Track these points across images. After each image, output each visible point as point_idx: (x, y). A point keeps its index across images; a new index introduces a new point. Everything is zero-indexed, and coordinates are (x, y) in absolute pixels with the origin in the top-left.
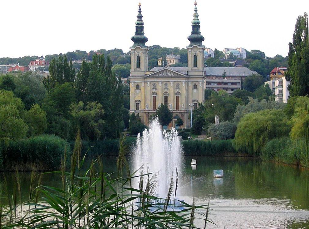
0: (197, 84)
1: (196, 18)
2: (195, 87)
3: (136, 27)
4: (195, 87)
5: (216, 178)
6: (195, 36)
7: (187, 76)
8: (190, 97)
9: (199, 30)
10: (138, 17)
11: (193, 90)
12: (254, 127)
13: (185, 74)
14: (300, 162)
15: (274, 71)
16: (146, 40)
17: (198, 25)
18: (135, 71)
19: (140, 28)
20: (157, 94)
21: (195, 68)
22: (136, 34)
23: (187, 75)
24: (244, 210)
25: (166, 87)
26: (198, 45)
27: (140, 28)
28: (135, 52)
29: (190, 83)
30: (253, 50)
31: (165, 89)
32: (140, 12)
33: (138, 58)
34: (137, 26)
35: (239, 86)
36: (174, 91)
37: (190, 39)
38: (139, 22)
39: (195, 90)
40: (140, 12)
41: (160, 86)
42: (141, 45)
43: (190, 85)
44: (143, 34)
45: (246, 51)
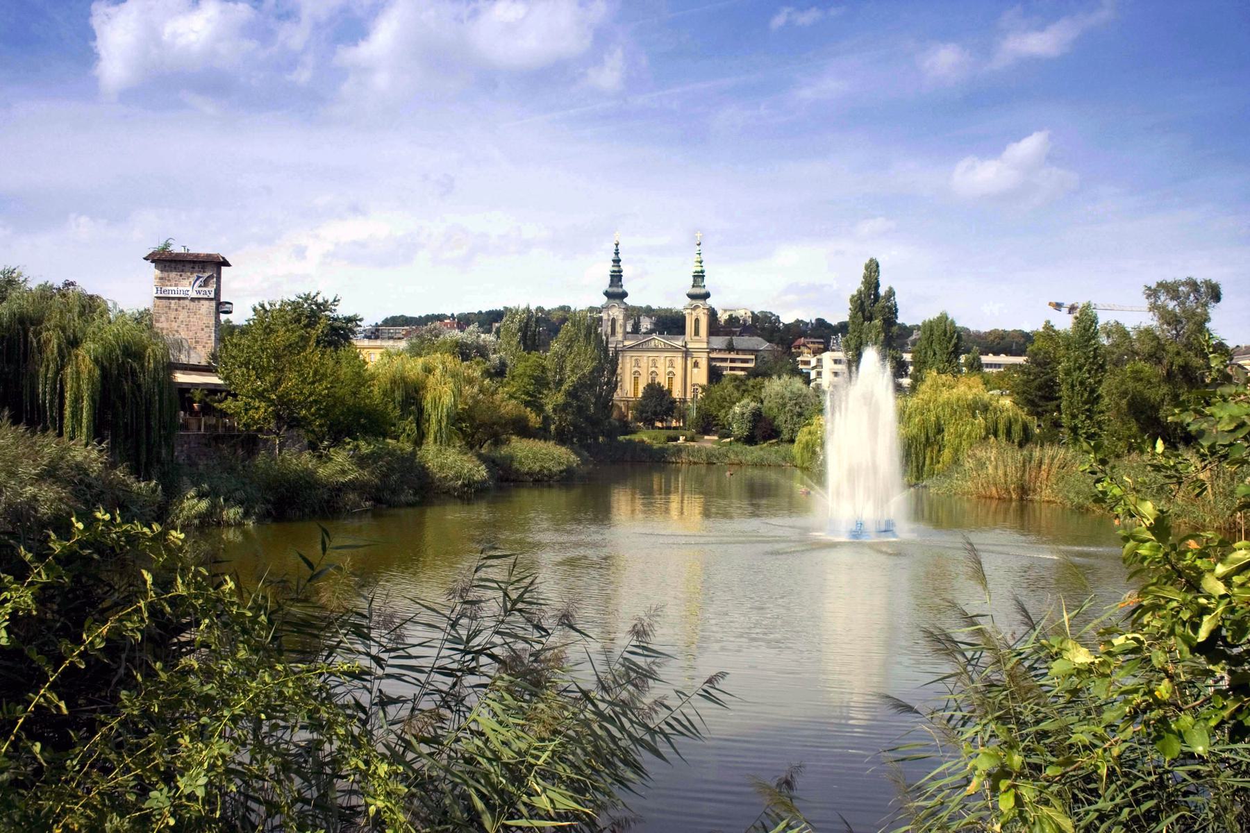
0: (699, 360)
2: (696, 365)
3: (612, 276)
5: (362, 543)
10: (614, 261)
12: (1176, 400)
14: (701, 493)
15: (796, 343)
16: (625, 295)
18: (692, 341)
19: (616, 278)
21: (697, 338)
22: (610, 286)
24: (774, 557)
25: (672, 366)
27: (616, 278)
30: (897, 310)
32: (617, 254)
33: (697, 321)
35: (751, 365)
37: (607, 294)
38: (616, 269)
39: (695, 370)
40: (617, 254)
41: (643, 363)
42: (617, 301)
43: (689, 362)
44: (622, 286)
45: (753, 313)
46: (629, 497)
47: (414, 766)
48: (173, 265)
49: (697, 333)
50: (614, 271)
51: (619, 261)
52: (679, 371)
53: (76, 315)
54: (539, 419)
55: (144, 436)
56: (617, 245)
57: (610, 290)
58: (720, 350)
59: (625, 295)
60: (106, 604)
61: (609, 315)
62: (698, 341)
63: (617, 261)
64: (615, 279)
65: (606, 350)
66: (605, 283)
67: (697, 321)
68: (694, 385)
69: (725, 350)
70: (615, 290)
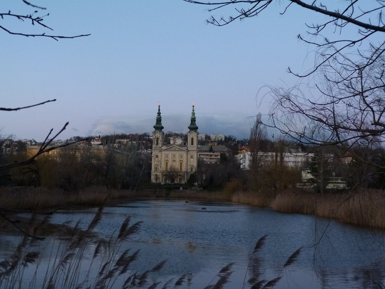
2: (192, 157)
16: (162, 128)
21: (192, 146)
37: (154, 127)
39: (192, 159)
43: (189, 156)
46: (292, 263)
48: (187, 165)
49: (192, 144)
50: (158, 118)
55: (75, 278)
57: (156, 126)
58: (206, 151)
59: (162, 128)
61: (156, 136)
62: (193, 148)
64: (158, 121)
67: (192, 139)
68: (191, 166)
69: (208, 151)
70: (158, 126)
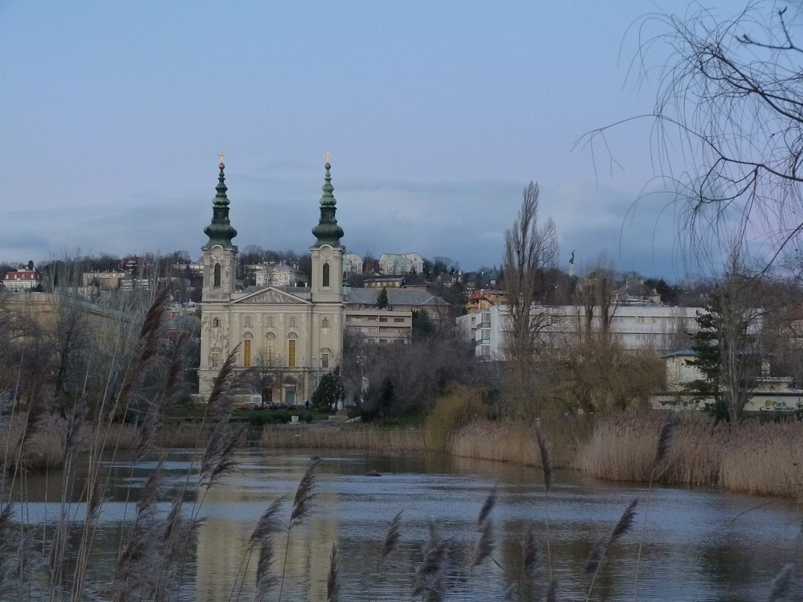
0: (329, 318)
1: (221, 194)
2: (325, 323)
3: (215, 208)
4: (325, 323)
6: (327, 228)
7: (310, 303)
8: (316, 343)
9: (334, 216)
11: (322, 330)
13: (307, 300)
16: (232, 234)
17: (331, 206)
20: (252, 336)
21: (326, 288)
22: (214, 222)
23: (311, 300)
26: (332, 245)
28: (321, 255)
29: (315, 316)
31: (267, 327)
32: (222, 179)
33: (326, 267)
34: (217, 206)
36: (285, 330)
38: (221, 200)
39: (325, 331)
40: (222, 179)
41: (257, 322)
42: (223, 242)
44: (228, 222)
47: (715, 402)
49: (326, 283)
50: (218, 203)
51: (225, 189)
52: (303, 334)
53: (131, 328)
54: (182, 391)
56: (222, 168)
58: (367, 306)
59: (232, 234)
60: (756, 390)
61: (212, 260)
63: (222, 190)
65: (165, 294)
66: (207, 217)
67: (326, 267)
68: (322, 350)
69: (374, 306)
70: (220, 227)
